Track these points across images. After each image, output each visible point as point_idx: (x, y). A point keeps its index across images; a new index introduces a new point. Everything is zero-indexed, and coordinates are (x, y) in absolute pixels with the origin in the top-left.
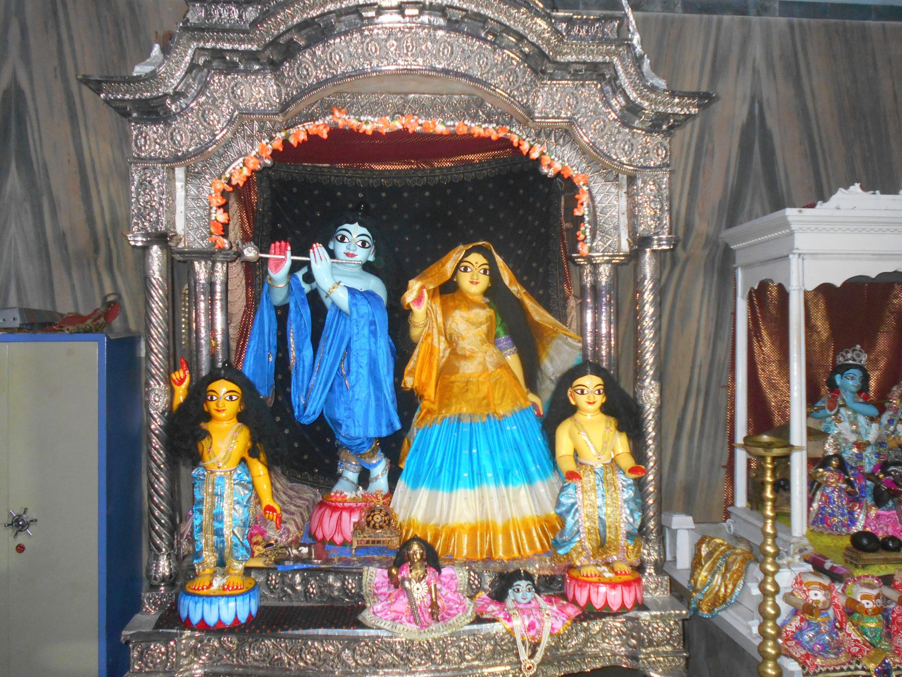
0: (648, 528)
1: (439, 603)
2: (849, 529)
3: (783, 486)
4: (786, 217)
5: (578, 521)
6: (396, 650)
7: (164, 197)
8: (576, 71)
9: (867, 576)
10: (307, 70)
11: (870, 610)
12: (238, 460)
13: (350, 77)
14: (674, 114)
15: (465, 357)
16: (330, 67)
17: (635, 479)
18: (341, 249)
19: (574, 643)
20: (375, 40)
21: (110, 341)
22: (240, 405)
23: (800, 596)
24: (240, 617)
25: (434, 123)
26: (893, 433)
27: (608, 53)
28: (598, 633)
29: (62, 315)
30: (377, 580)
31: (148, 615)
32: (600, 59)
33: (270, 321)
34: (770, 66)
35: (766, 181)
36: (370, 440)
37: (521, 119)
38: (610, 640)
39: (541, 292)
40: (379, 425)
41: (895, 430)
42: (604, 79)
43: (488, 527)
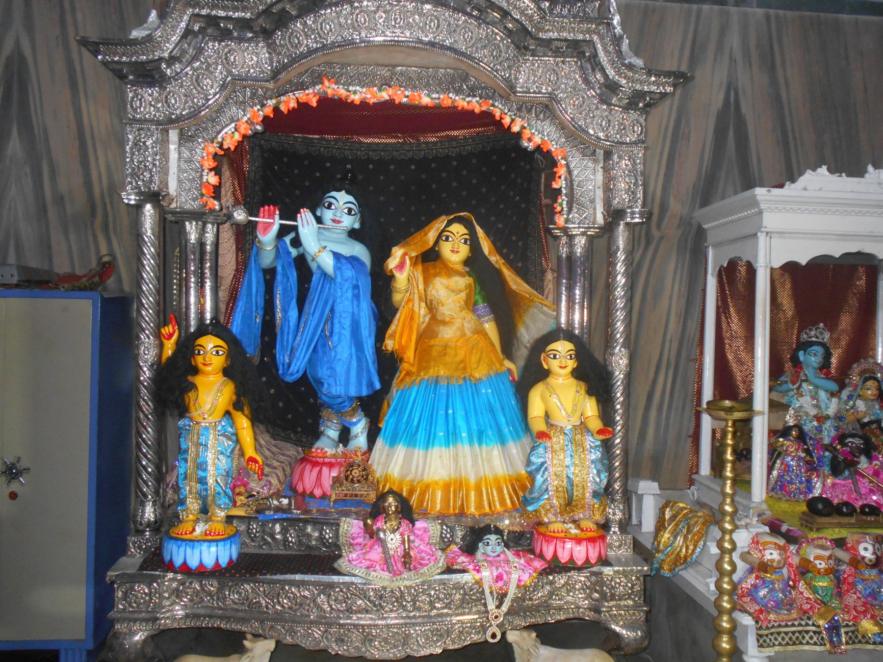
0: (614, 488)
1: (412, 553)
2: (806, 496)
3: (744, 455)
4: (755, 196)
5: (546, 479)
6: (370, 597)
7: (158, 157)
8: (557, 48)
9: (821, 538)
10: (298, 39)
11: (822, 570)
12: (222, 413)
13: (338, 46)
14: (650, 92)
15: (444, 323)
16: (320, 36)
17: (602, 441)
18: (328, 215)
19: (539, 595)
20: (365, 12)
21: (105, 301)
22: (226, 360)
23: (756, 555)
24: (221, 562)
25: (419, 95)
26: (852, 408)
27: (588, 31)
28: (563, 586)
29: (58, 275)
30: (353, 531)
31: (133, 559)
32: (580, 37)
33: (258, 282)
34: (746, 53)
35: (739, 162)
36: (351, 399)
37: (503, 93)
38: (574, 593)
39: (520, 265)
40: (360, 384)
41: (854, 404)
42: (584, 56)
43: (461, 484)
